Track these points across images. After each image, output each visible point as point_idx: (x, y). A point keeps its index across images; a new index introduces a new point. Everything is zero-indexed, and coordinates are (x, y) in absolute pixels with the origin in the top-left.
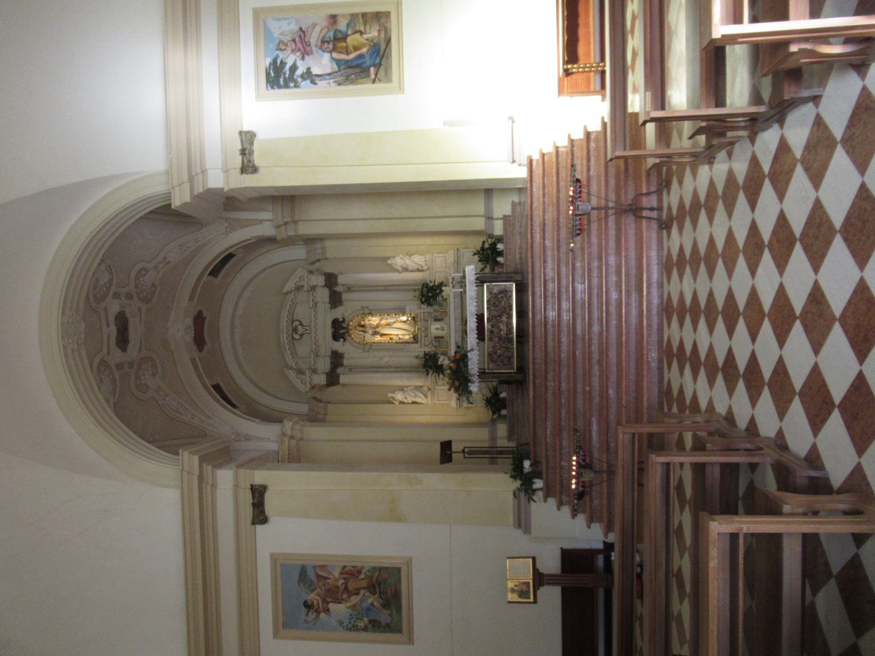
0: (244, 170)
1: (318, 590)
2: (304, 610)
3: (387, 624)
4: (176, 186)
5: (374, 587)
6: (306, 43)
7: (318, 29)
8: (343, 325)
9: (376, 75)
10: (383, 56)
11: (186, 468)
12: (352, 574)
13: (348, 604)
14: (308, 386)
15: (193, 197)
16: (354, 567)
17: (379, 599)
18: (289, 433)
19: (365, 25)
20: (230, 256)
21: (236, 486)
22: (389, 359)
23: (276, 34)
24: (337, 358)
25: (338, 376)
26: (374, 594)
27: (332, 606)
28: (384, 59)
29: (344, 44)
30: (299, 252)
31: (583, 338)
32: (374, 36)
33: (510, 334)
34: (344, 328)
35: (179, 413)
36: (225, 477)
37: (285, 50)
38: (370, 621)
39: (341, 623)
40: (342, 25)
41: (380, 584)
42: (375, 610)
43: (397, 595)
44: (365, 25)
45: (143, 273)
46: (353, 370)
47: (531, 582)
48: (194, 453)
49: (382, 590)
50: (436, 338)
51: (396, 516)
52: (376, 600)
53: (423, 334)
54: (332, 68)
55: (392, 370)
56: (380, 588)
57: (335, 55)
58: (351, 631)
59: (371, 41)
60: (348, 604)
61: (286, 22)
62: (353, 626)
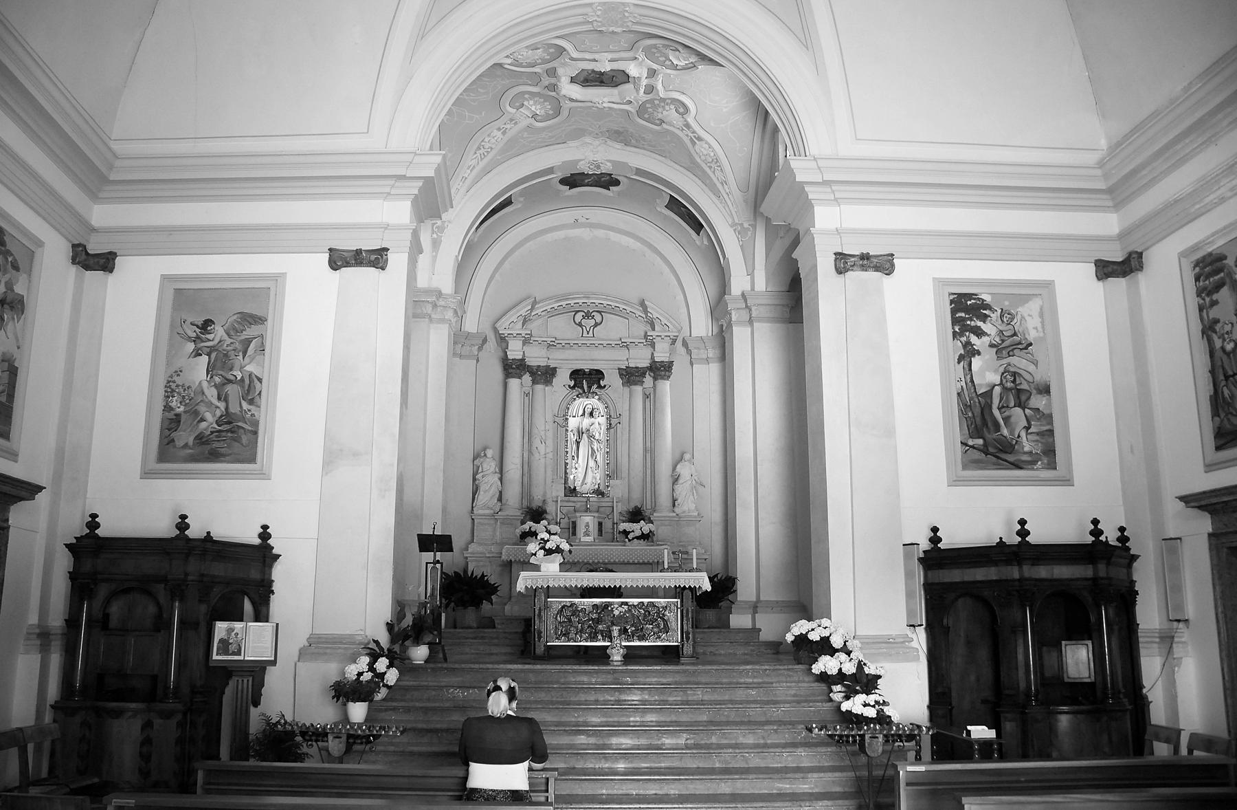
0: (840, 256)
1: (229, 341)
2: (200, 321)
3: (173, 441)
4: (818, 165)
5: (229, 423)
6: (1013, 350)
7: (1031, 368)
8: (595, 386)
9: (972, 447)
10: (998, 458)
11: (417, 159)
12: (248, 391)
13: (205, 384)
14: (506, 332)
15: (802, 185)
16: (260, 394)
17: (210, 430)
18: (441, 303)
19: (1038, 434)
20: (697, 227)
21: (386, 227)
22: (542, 452)
23: (1023, 310)
24: (545, 375)
25: (520, 377)
26: (217, 422)
27: (205, 359)
28: (994, 459)
29: (1012, 404)
30: (702, 326)
31: (605, 747)
32: (1023, 447)
33: (603, 636)
34: (590, 388)
35: (479, 148)
36: (399, 212)
37: (1003, 321)
38: (178, 415)
39: (178, 373)
40: (1037, 401)
41: (232, 432)
42: (195, 423)
43: (214, 456)
44: (1038, 434)
45: (681, 110)
46: (526, 398)
47: (241, 658)
48: (438, 170)
49: (224, 434)
50: (574, 524)
51: (331, 459)
52: (209, 426)
53: (578, 505)
54: (981, 385)
55: (526, 455)
56: (227, 431)
57: (997, 390)
58: (166, 387)
59: (1017, 441)
60: (205, 384)
61: (1039, 326)
62: (173, 391)
